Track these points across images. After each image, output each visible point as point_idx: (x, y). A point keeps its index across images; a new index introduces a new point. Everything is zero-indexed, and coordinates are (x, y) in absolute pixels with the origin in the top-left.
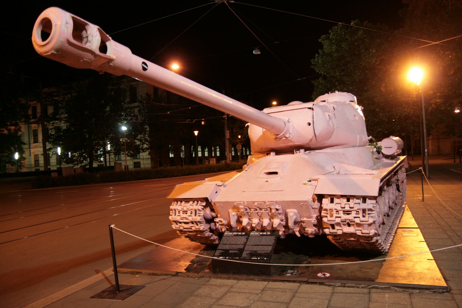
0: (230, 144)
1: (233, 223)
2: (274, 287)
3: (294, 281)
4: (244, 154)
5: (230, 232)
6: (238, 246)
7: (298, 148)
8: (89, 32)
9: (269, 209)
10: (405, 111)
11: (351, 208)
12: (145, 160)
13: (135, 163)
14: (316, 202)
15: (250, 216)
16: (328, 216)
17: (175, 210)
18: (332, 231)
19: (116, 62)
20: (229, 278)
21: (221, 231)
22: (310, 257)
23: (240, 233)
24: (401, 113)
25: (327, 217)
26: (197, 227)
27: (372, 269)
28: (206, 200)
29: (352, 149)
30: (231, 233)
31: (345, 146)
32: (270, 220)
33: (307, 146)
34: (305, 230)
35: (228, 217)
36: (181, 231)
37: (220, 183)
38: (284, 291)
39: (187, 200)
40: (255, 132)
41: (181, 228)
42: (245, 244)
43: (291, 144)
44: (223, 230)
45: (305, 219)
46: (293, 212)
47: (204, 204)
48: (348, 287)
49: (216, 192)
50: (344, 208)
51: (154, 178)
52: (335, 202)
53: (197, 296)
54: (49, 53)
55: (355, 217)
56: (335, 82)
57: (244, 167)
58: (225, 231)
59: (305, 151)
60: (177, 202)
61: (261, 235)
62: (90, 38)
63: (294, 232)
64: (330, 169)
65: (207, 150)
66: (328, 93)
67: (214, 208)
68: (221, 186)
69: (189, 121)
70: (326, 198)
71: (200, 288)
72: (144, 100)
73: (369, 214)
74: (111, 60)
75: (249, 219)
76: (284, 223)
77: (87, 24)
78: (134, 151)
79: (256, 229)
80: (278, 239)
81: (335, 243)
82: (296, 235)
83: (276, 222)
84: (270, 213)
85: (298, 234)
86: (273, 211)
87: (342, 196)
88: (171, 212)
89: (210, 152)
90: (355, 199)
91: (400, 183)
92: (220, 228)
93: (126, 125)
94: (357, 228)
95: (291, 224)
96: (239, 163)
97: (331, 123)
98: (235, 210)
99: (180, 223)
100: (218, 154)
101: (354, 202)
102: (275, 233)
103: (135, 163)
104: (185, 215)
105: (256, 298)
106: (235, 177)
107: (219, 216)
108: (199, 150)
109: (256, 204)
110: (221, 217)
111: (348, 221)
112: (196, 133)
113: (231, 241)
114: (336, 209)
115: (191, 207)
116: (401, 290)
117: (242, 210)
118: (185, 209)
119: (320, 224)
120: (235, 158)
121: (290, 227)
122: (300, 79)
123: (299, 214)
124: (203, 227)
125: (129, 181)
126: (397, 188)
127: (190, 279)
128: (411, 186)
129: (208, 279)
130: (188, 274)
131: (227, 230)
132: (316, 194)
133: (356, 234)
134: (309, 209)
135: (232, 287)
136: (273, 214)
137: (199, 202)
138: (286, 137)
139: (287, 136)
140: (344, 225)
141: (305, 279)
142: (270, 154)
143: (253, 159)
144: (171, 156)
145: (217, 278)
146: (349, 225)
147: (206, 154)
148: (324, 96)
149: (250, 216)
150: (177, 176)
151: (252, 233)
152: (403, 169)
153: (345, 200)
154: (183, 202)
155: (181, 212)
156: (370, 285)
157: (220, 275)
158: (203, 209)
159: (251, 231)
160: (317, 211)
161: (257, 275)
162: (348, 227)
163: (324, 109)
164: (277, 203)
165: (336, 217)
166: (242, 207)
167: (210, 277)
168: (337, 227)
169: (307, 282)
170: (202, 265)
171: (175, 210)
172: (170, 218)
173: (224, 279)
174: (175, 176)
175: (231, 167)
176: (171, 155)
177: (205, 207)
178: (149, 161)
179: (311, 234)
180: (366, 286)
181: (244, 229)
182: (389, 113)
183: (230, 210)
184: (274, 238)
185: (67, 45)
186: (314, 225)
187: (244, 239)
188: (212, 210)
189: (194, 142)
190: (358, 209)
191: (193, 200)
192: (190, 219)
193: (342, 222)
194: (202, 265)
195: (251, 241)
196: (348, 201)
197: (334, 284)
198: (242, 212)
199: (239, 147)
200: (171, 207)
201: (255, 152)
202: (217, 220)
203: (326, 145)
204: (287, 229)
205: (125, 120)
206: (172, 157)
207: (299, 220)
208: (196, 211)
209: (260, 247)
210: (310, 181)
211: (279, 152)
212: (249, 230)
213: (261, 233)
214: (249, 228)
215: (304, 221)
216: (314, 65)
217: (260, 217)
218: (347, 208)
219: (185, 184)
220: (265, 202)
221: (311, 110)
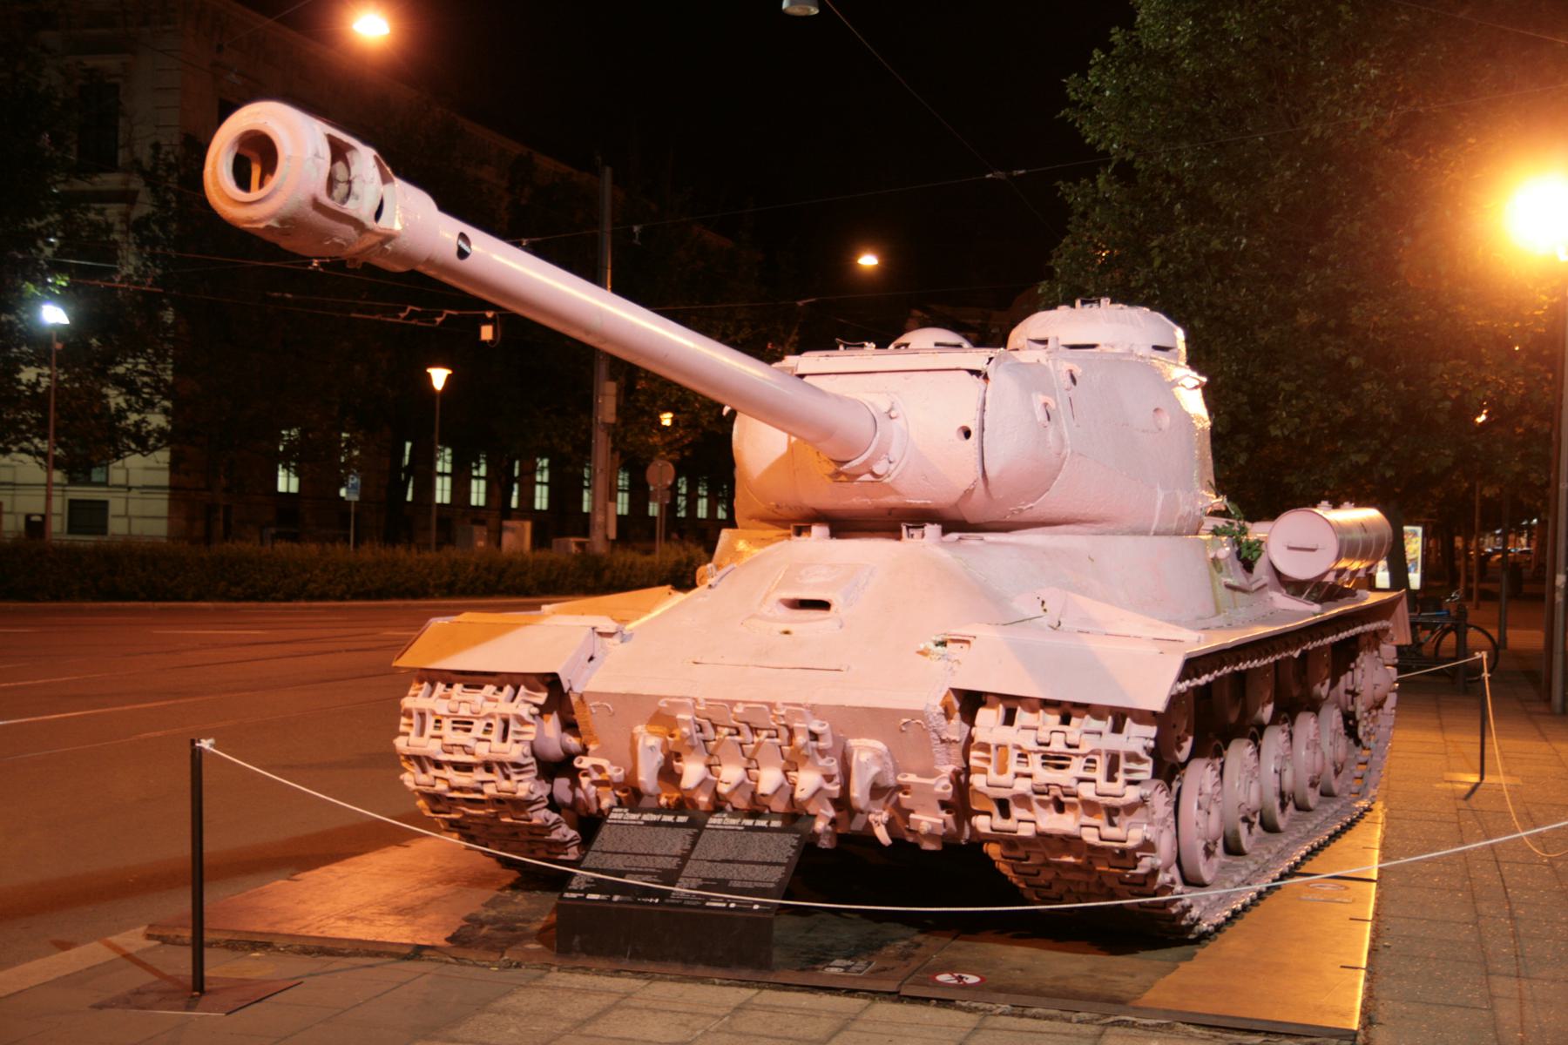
0: (613, 450)
1: (647, 776)
2: (779, 1003)
3: (851, 992)
4: (682, 514)
5: (631, 811)
6: (659, 860)
7: (919, 517)
8: (354, 170)
9: (784, 733)
10: (1484, 383)
11: (1070, 746)
12: (138, 492)
13: (74, 505)
14: (956, 719)
15: (711, 755)
16: (991, 768)
17: (422, 715)
18: (999, 822)
19: (400, 241)
20: (617, 973)
21: (594, 808)
22: (921, 932)
23: (669, 818)
24: (1465, 391)
25: (984, 771)
26: (505, 785)
27: (1132, 976)
28: (551, 682)
29: (1128, 541)
30: (634, 816)
31: (1104, 526)
32: (785, 772)
33: (954, 514)
34: (907, 821)
35: (627, 756)
36: (435, 799)
37: (607, 625)
38: (814, 1014)
39: (474, 680)
40: (758, 447)
41: (441, 787)
42: (685, 858)
43: (891, 500)
44: (605, 803)
45: (911, 778)
46: (872, 749)
47: (541, 698)
48: (1034, 1017)
49: (591, 659)
50: (1048, 744)
51: (198, 597)
52: (1017, 723)
53: (504, 1012)
54: (261, 226)
55: (1081, 780)
56: (1172, 204)
57: (701, 571)
58: (610, 809)
59: (945, 532)
60: (433, 685)
61: (747, 828)
62: (356, 187)
63: (869, 825)
64: (1025, 606)
65: (483, 471)
66: (1073, 306)
67: (578, 717)
68: (610, 635)
69: (412, 315)
70: (993, 707)
71: (510, 993)
72: (170, 168)
73: (1128, 771)
74: (389, 237)
75: (709, 766)
76: (834, 788)
77: (350, 148)
78: (86, 442)
79: (728, 807)
80: (809, 846)
81: (1010, 874)
82: (875, 839)
83: (807, 781)
84: (786, 748)
85: (882, 835)
86: (801, 739)
87: (1047, 704)
88: (404, 720)
89: (499, 485)
90: (1087, 717)
91: (1360, 708)
92: (592, 796)
93: (63, 298)
94: (1086, 820)
95: (859, 792)
96: (656, 558)
97: (1050, 437)
98: (657, 729)
99: (438, 765)
100: (541, 500)
101: (1085, 727)
102: (798, 825)
103: (74, 505)
104: (460, 737)
105: (714, 1025)
106: (663, 608)
107: (592, 747)
108: (439, 468)
109: (739, 709)
110: (600, 753)
111: (1055, 791)
112: (439, 377)
113: (634, 848)
114: (1019, 747)
115: (489, 707)
116: (1206, 1033)
117: (686, 730)
118: (464, 711)
119: (960, 802)
120: (634, 529)
121: (854, 804)
122: (1000, 175)
123: (893, 760)
124: (525, 786)
125: (57, 598)
126: (1346, 726)
127: (471, 970)
128: (1456, 738)
129: (539, 972)
130: (460, 953)
131: (620, 804)
132: (956, 691)
133: (1080, 838)
134: (929, 740)
135: (628, 995)
136: (797, 751)
137: (523, 689)
138: (873, 474)
139: (878, 469)
140: (1043, 804)
141: (891, 986)
142: (808, 530)
143: (741, 545)
144: (282, 487)
145: (573, 970)
146: (1060, 807)
147: (478, 494)
148: (1052, 313)
149: (711, 755)
150: (323, 597)
151: (714, 821)
152: (1388, 650)
153: (1053, 719)
154: (458, 687)
155: (447, 724)
156: (1108, 1016)
157: (583, 961)
158: (533, 716)
159: (710, 813)
160: (956, 751)
161: (721, 966)
162: (1056, 815)
163: (1033, 379)
164: (815, 710)
165: (1017, 775)
166: (687, 717)
167: (547, 967)
168: (1017, 812)
169: (897, 997)
170: (514, 930)
171: (422, 715)
172: (400, 743)
173: (599, 973)
174: (311, 598)
175: (608, 575)
176: (286, 482)
177: (544, 710)
178: (160, 505)
179: (930, 836)
180: (1096, 1016)
181: (683, 804)
182: (1407, 384)
183: (640, 729)
184: (795, 842)
185: (309, 209)
186: (944, 805)
187: (677, 842)
188: (569, 726)
189: (423, 419)
190: (1092, 752)
191: (499, 679)
192: (482, 751)
193: (1036, 793)
194: (514, 930)
195: (709, 847)
196: (1066, 720)
197: (988, 1006)
198: (684, 738)
199: (661, 473)
200: (408, 702)
201: (751, 518)
202: (584, 763)
203: (1028, 516)
204: (845, 813)
205: (57, 268)
206: (287, 494)
207: (891, 782)
208: (506, 723)
209: (741, 867)
210: (943, 644)
211: (844, 525)
212: (702, 808)
213: (749, 822)
214: (703, 799)
215: (908, 786)
216: (1075, 104)
217: (750, 760)
218: (1057, 746)
219: (466, 617)
220: (772, 706)
221: (980, 380)
